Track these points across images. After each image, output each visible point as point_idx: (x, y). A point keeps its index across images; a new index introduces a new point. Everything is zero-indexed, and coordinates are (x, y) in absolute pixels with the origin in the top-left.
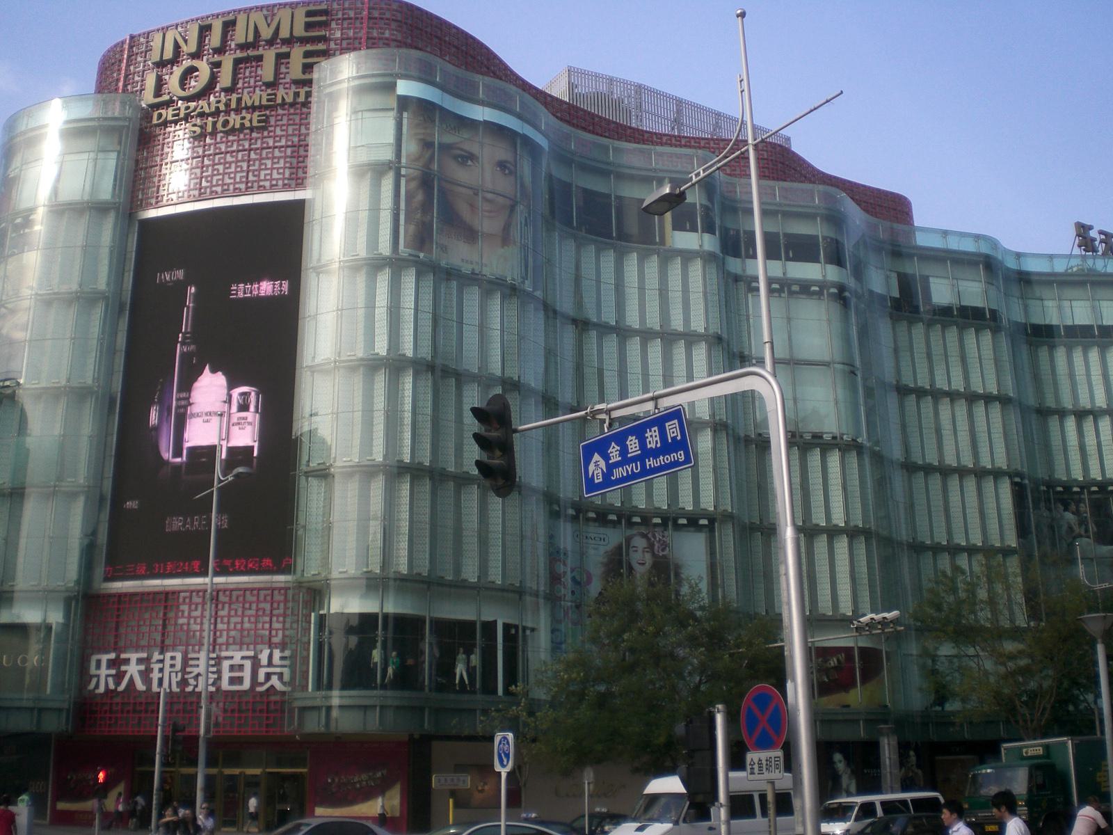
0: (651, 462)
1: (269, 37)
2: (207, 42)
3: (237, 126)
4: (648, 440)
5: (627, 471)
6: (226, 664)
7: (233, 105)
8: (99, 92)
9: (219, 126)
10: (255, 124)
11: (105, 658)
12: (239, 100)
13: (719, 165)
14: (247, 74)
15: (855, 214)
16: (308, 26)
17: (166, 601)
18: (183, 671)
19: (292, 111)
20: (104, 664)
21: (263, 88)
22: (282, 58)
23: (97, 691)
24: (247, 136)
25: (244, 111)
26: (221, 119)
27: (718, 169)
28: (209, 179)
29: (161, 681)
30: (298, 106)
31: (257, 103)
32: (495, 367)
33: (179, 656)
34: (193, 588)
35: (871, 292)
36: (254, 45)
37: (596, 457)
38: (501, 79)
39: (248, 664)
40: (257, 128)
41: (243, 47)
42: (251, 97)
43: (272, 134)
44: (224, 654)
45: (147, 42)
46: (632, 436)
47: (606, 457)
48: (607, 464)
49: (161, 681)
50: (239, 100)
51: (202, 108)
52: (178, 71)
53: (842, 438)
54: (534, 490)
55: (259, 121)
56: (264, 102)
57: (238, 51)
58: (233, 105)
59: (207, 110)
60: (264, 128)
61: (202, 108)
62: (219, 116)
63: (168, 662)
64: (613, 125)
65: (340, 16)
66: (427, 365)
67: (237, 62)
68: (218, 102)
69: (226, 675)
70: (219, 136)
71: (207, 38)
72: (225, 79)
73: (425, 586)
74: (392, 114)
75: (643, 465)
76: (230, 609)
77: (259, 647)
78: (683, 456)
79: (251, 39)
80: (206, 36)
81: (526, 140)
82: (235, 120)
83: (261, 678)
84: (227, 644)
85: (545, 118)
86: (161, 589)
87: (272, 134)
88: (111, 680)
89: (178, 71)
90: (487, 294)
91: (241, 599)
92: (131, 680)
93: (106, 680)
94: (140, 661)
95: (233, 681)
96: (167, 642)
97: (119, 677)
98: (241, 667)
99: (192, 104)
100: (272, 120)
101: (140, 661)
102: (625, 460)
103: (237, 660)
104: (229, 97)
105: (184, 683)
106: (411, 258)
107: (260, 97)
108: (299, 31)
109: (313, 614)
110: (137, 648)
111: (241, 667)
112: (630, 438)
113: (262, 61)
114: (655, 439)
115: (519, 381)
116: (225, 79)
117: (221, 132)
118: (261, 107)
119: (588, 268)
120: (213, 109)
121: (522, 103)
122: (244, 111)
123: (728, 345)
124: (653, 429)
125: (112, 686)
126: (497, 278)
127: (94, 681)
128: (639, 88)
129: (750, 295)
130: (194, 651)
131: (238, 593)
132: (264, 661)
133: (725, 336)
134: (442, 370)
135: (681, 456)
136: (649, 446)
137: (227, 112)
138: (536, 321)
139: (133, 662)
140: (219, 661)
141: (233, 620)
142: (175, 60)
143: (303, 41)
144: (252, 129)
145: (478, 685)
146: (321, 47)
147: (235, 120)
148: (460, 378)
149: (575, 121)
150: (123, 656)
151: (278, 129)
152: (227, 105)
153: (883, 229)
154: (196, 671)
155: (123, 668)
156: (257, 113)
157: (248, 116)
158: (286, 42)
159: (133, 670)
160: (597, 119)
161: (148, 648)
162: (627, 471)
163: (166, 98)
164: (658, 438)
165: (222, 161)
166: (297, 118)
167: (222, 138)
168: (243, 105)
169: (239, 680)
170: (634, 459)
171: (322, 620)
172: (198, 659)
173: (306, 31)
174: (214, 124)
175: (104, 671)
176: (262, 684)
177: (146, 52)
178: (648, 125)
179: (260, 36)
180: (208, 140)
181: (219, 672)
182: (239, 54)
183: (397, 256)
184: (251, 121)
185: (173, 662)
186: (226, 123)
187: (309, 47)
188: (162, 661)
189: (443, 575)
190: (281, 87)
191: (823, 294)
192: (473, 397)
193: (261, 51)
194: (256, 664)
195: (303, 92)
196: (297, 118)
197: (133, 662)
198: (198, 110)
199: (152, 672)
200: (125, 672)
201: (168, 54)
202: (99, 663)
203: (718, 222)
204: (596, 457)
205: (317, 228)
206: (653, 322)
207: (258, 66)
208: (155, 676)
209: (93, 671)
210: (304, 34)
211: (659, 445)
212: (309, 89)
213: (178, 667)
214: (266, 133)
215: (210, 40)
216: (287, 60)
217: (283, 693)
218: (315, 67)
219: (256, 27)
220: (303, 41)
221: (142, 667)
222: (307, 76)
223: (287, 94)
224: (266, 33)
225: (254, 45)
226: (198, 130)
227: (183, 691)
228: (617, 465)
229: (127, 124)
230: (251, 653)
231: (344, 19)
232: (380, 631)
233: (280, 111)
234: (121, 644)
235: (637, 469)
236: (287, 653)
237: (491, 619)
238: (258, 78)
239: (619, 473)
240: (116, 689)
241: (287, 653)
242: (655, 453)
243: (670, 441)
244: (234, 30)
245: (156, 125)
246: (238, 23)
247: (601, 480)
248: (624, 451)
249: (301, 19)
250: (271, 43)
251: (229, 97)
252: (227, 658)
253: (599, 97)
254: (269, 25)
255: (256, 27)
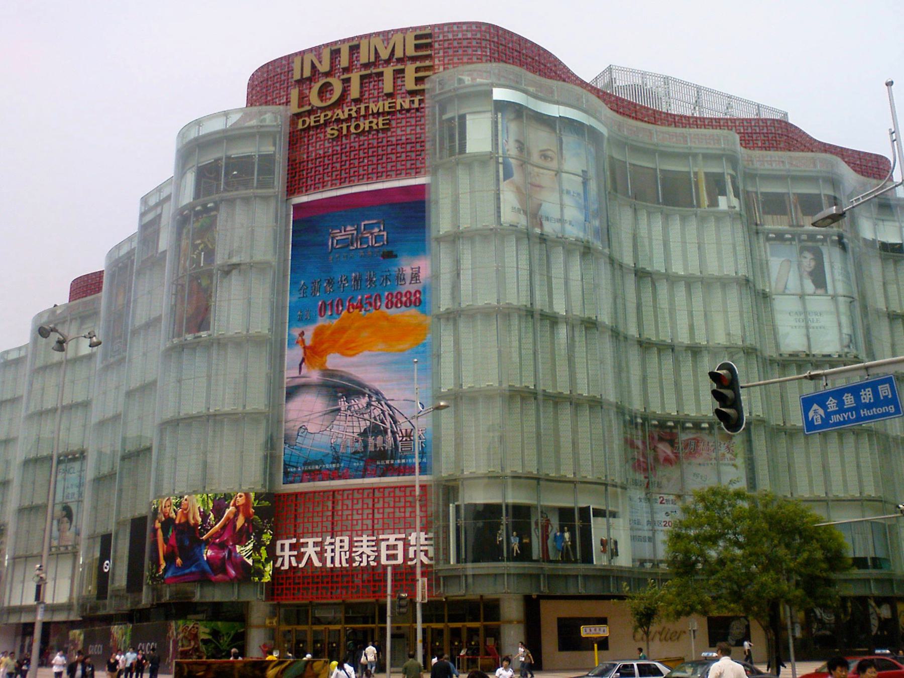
0: (865, 412)
1: (387, 57)
2: (337, 63)
3: (367, 129)
4: (862, 397)
5: (844, 418)
6: (383, 545)
7: (363, 112)
8: (251, 105)
9: (353, 130)
10: (381, 126)
11: (287, 543)
12: (367, 108)
13: (877, 194)
14: (371, 87)
15: (849, 176)
16: (417, 47)
17: (333, 496)
18: (351, 552)
19: (408, 115)
20: (287, 547)
21: (385, 98)
22: (399, 73)
23: (282, 568)
24: (375, 136)
25: (371, 117)
26: (353, 124)
27: (875, 196)
28: (347, 171)
29: (333, 559)
30: (412, 111)
31: (381, 111)
32: (577, 311)
33: (346, 539)
34: (353, 487)
35: (865, 239)
36: (374, 64)
37: (815, 406)
38: (564, 81)
39: (400, 545)
40: (382, 129)
41: (366, 66)
42: (376, 106)
43: (394, 134)
44: (381, 537)
45: (288, 64)
46: (848, 393)
47: (824, 406)
48: (825, 412)
49: (333, 559)
50: (367, 108)
51: (338, 115)
52: (316, 87)
53: (846, 356)
54: (610, 404)
55: (383, 124)
56: (387, 109)
57: (363, 69)
58: (363, 112)
59: (342, 117)
60: (388, 130)
61: (338, 115)
62: (351, 122)
63: (338, 544)
64: (613, 98)
65: (441, 38)
66: (527, 311)
67: (362, 77)
68: (350, 110)
69: (384, 553)
70: (353, 137)
71: (337, 60)
72: (355, 92)
73: (535, 482)
74: (489, 115)
75: (858, 413)
76: (363, 503)
77: (408, 531)
78: (893, 409)
79: (372, 59)
80: (336, 58)
81: (591, 130)
82: (365, 125)
83: (411, 555)
84: (383, 529)
85: (606, 111)
86: (330, 488)
87: (394, 134)
88: (293, 559)
89: (316, 87)
90: (568, 252)
91: (392, 494)
92: (310, 558)
93: (290, 560)
94: (316, 544)
95: (389, 557)
96: (336, 529)
97: (299, 558)
98: (395, 547)
99: (330, 113)
100: (393, 123)
101: (316, 544)
102: (841, 410)
103: (392, 542)
104: (358, 106)
105: (350, 560)
106: (511, 228)
107: (383, 105)
108: (411, 52)
109: (451, 505)
110: (313, 534)
111: (395, 547)
112: (846, 395)
113: (382, 76)
114: (868, 397)
115: (596, 320)
116: (355, 92)
117: (354, 133)
118: (383, 114)
119: (643, 231)
120: (346, 116)
121: (587, 101)
122: (371, 117)
123: (754, 286)
124: (867, 390)
125: (294, 564)
126: (511, 225)
127: (280, 560)
128: (666, 80)
129: (767, 244)
130: (357, 535)
131: (390, 489)
132: (413, 542)
133: (751, 278)
134: (541, 315)
135: (892, 409)
136: (863, 401)
137: (357, 118)
138: (604, 272)
139: (311, 544)
140: (378, 542)
141: (387, 510)
142: (310, 79)
143: (414, 59)
144: (377, 131)
145: (578, 557)
146: (427, 63)
147: (365, 125)
148: (553, 320)
149: (621, 110)
150: (302, 540)
151: (399, 130)
152: (358, 111)
153: (872, 186)
154: (360, 550)
155: (302, 550)
156: (381, 119)
157: (375, 121)
158: (400, 60)
159: (310, 551)
160: (638, 107)
161: (322, 534)
162: (844, 418)
163: (307, 108)
164: (871, 396)
165: (356, 156)
166: (413, 121)
167: (355, 138)
168: (370, 112)
169: (394, 557)
170: (850, 410)
171: (458, 508)
172: (362, 541)
173: (416, 51)
174: (348, 127)
175: (287, 553)
176: (411, 560)
177: (289, 72)
178: (676, 109)
179: (379, 57)
180: (344, 141)
181: (378, 551)
182: (364, 72)
183: (501, 227)
184: (377, 124)
185: (342, 544)
186: (357, 126)
187: (418, 64)
188: (332, 544)
189: (548, 472)
190: (399, 96)
191: (826, 241)
192: (708, 365)
193: (380, 69)
194: (407, 545)
195: (417, 99)
196: (413, 121)
197: (311, 544)
198: (335, 117)
199: (326, 552)
200: (304, 553)
201: (307, 73)
202: (283, 545)
203: (741, 187)
204: (815, 406)
205: (433, 206)
206: (694, 269)
207: (379, 81)
208: (328, 555)
209: (278, 553)
210: (414, 54)
211: (872, 401)
212: (422, 98)
213: (346, 548)
214: (389, 134)
215: (339, 61)
216: (402, 75)
217: (431, 566)
218: (426, 80)
219: (376, 49)
220: (414, 59)
221: (318, 549)
222: (419, 87)
223: (404, 101)
224: (384, 55)
225: (374, 64)
226: (336, 133)
227: (351, 565)
228: (835, 413)
229: (279, 130)
230: (403, 536)
231: (445, 40)
232: (504, 518)
233: (399, 116)
234: (300, 531)
235: (852, 416)
236: (431, 535)
237: (585, 505)
238: (380, 90)
239: (835, 418)
240: (298, 566)
241: (431, 535)
242: (869, 406)
243: (882, 398)
244: (358, 53)
245: (302, 130)
246: (361, 46)
247: (820, 423)
248: (841, 403)
249: (411, 43)
250: (388, 62)
251: (358, 106)
252: (383, 540)
253: (634, 89)
254: (386, 48)
255: (376, 49)
